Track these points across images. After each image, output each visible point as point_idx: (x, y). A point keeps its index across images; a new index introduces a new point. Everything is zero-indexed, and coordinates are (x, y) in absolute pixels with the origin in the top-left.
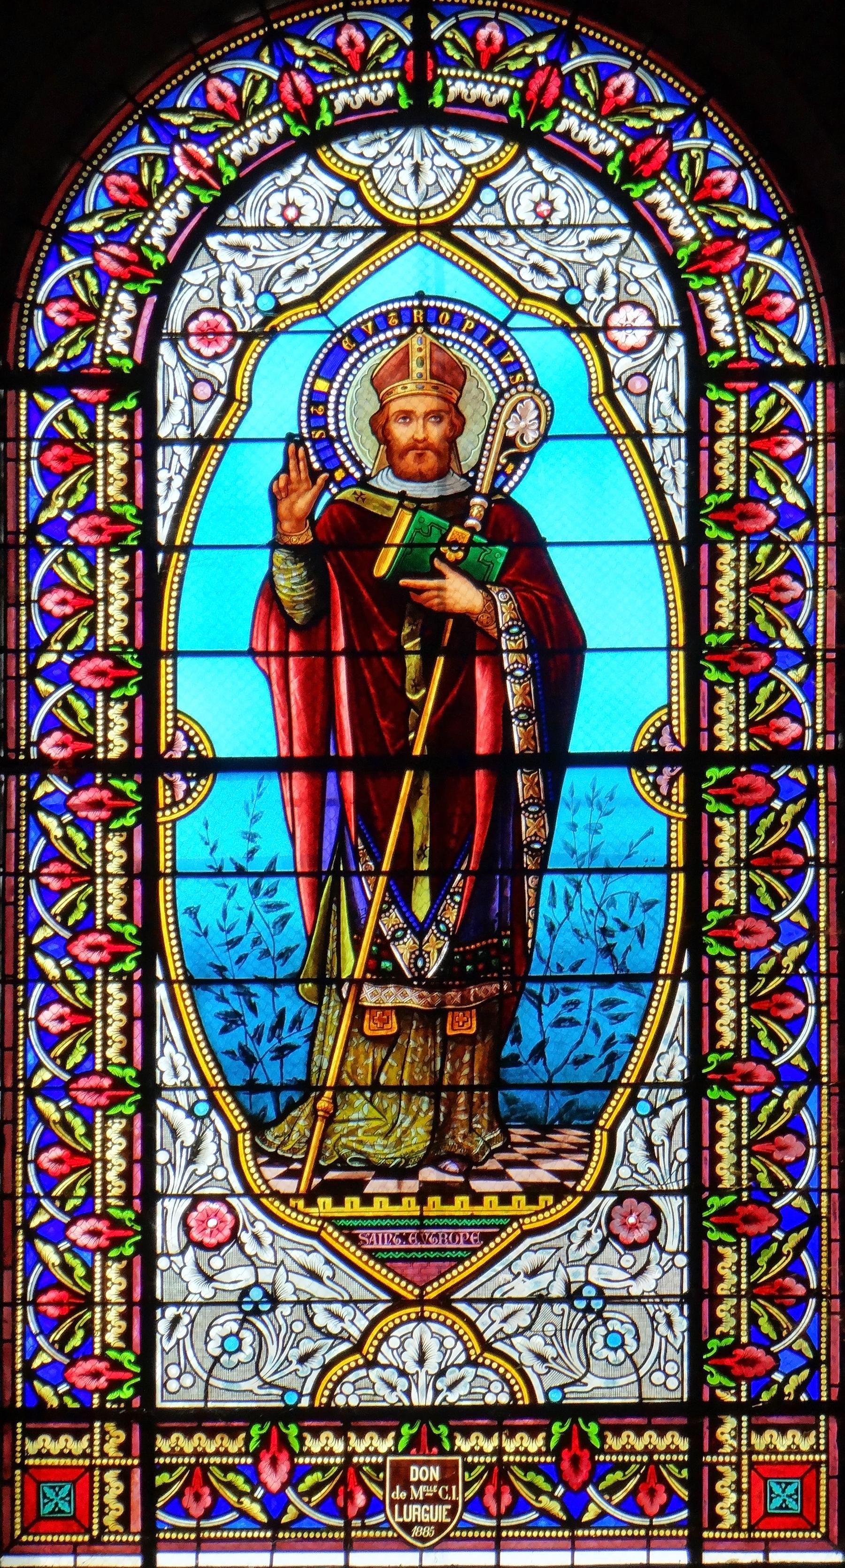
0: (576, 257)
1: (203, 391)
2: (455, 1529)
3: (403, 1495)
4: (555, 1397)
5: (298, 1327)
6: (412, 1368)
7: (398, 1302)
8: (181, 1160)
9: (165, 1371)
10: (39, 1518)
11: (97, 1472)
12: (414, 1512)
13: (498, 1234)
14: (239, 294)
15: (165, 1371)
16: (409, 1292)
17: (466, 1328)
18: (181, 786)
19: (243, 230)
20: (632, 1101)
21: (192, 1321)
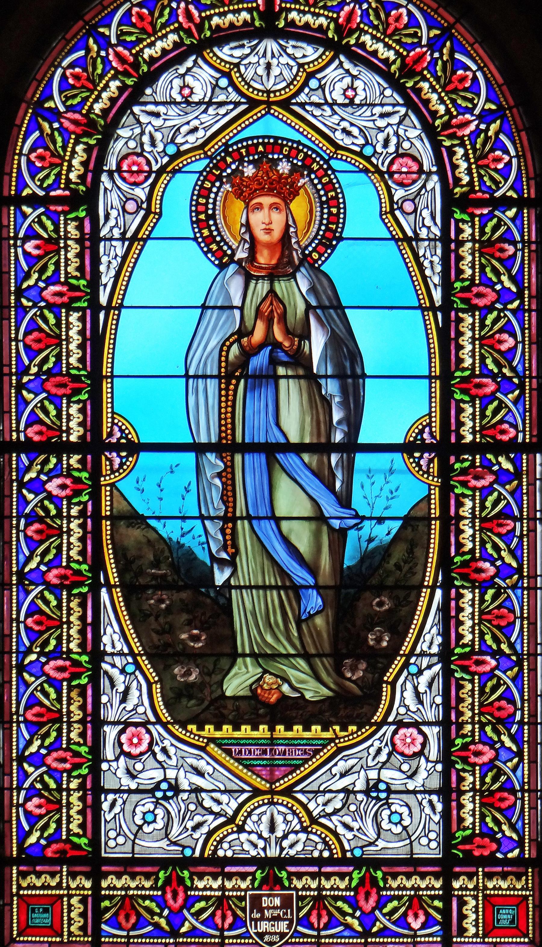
0: (370, 124)
1: (131, 206)
2: (291, 937)
3: (258, 916)
4: (358, 853)
5: (192, 807)
6: (266, 835)
7: (256, 792)
8: (116, 701)
9: (107, 834)
10: (28, 926)
11: (65, 899)
12: (264, 926)
13: (321, 750)
14: (153, 143)
15: (107, 834)
16: (264, 785)
17: (301, 809)
18: (117, 461)
19: (156, 104)
20: (406, 665)
21: (124, 803)
